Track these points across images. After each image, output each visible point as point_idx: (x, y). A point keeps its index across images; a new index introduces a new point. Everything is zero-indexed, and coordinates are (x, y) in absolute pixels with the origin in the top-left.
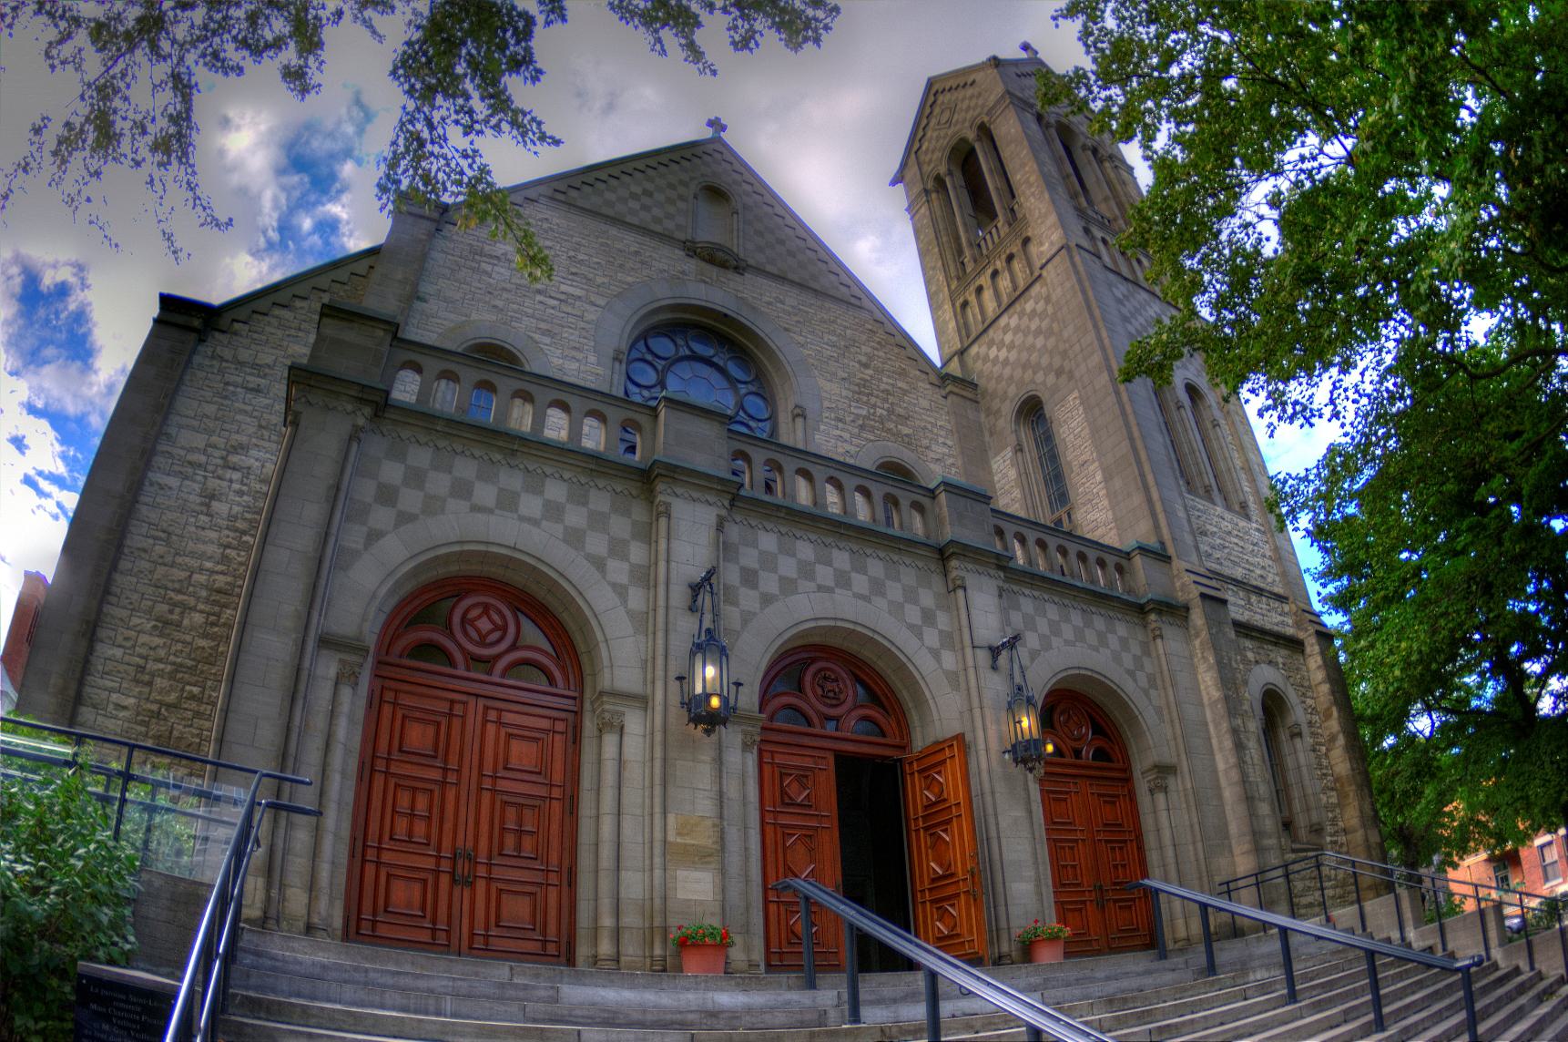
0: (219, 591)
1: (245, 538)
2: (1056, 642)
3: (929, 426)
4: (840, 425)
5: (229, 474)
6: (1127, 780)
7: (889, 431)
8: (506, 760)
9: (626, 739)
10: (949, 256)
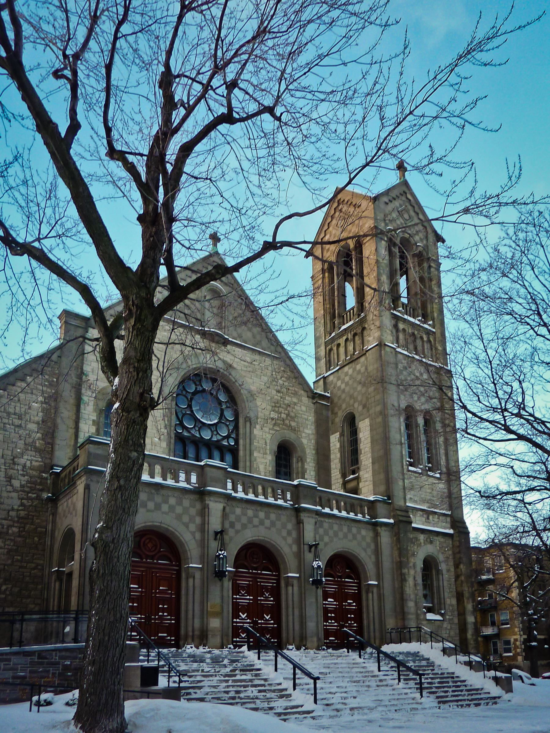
0: (22, 518)
2: (335, 539)
7: (286, 425)
9: (196, 580)
10: (328, 318)
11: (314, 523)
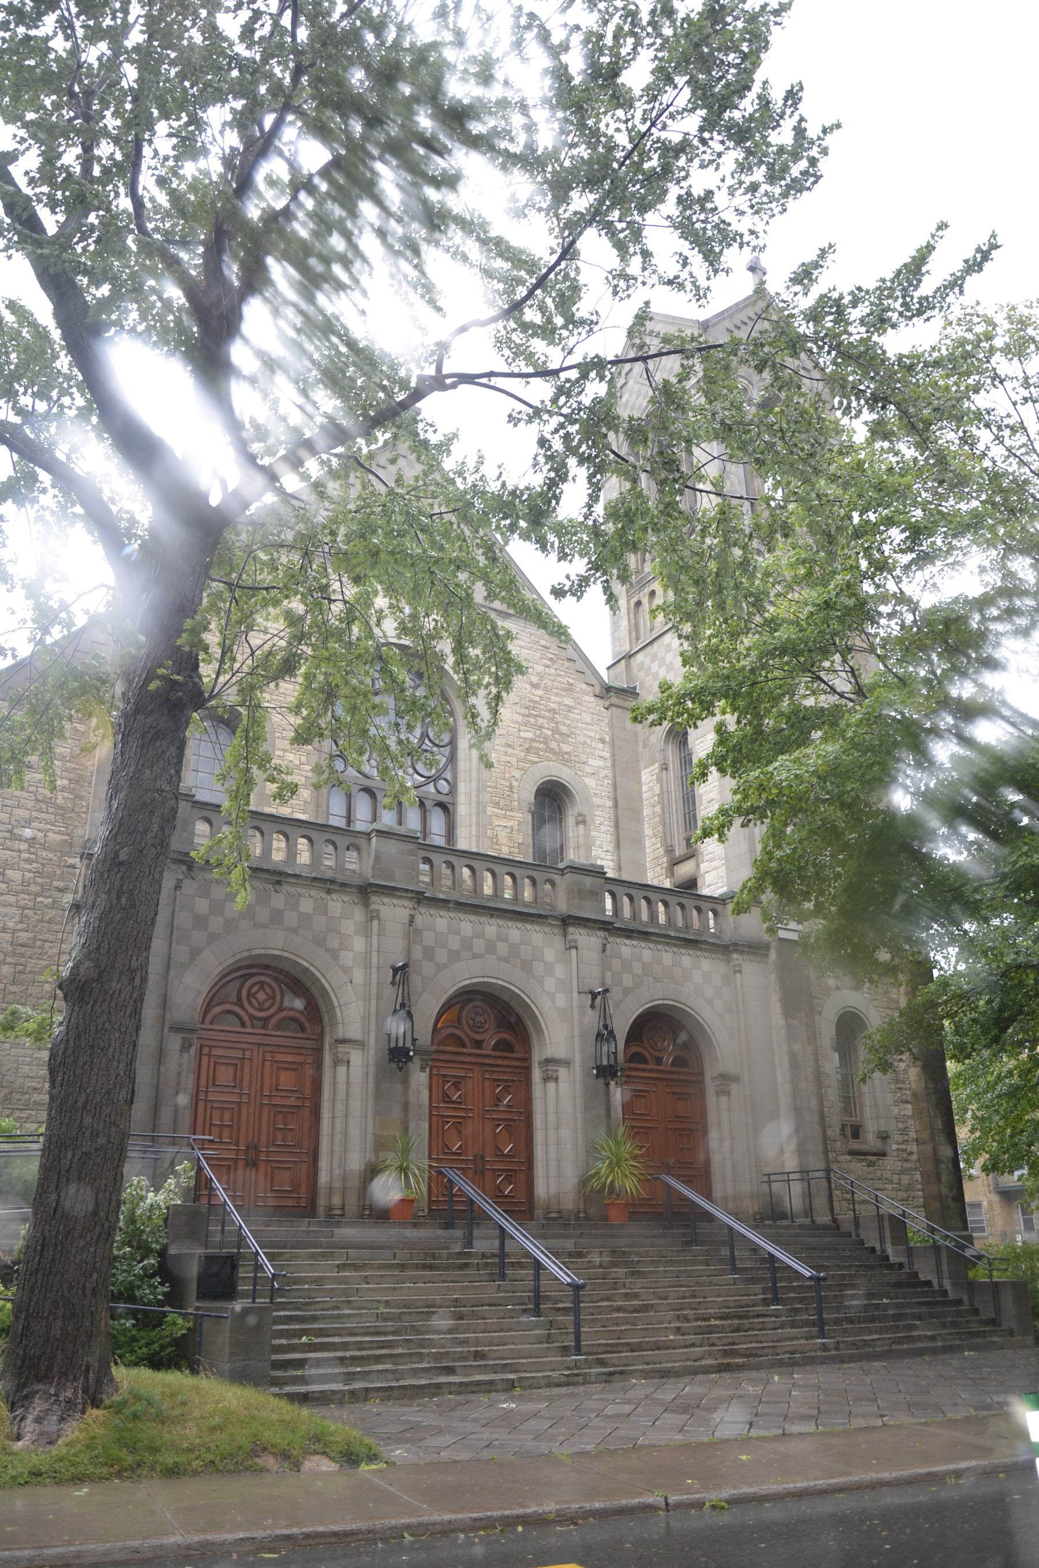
1: (39, 899)
3: (588, 741)
4: (510, 751)
5: (16, 845)
7: (552, 750)
8: (277, 1085)
9: (352, 1069)
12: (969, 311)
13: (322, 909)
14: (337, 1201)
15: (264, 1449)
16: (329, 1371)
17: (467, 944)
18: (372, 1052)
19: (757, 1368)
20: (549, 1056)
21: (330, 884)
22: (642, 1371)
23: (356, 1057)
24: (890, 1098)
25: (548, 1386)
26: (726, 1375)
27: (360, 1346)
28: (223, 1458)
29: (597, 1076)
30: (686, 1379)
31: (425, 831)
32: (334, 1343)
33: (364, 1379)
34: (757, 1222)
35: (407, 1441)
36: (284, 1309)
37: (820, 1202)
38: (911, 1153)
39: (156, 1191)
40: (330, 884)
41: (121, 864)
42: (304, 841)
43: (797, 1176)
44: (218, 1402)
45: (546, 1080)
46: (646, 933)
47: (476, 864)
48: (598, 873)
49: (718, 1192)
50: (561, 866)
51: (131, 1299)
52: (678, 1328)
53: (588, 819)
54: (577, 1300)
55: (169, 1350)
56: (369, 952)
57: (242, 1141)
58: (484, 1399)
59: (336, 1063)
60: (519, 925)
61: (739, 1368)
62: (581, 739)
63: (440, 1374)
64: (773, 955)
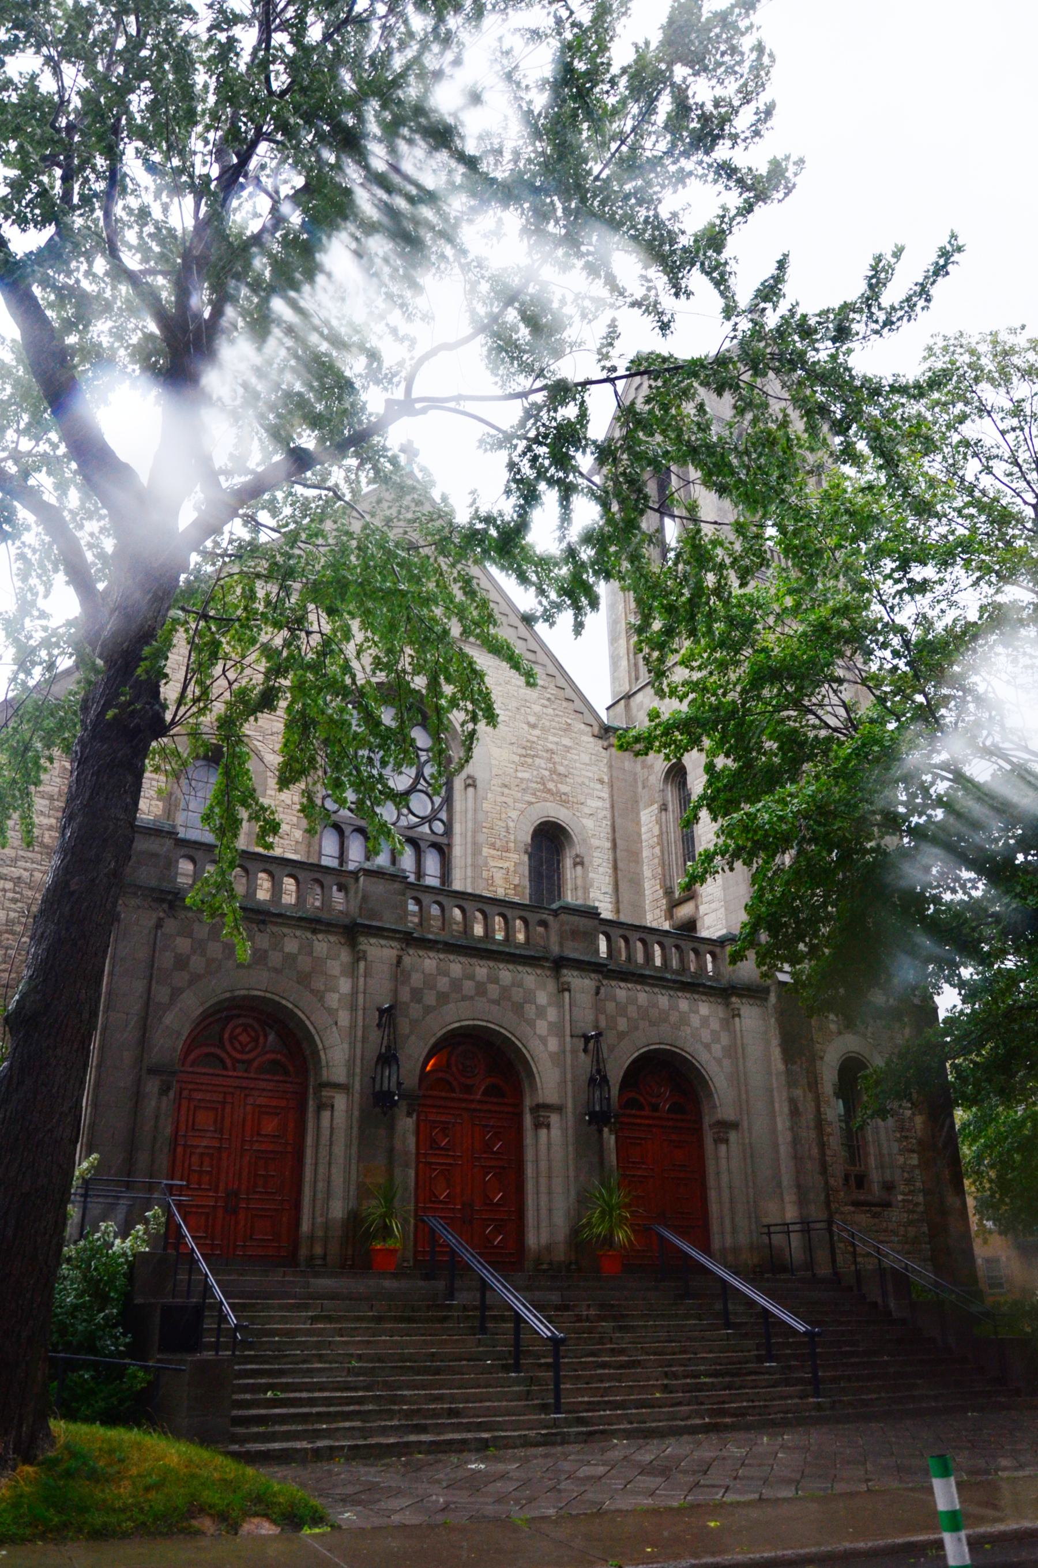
3: (587, 782)
4: (506, 791)
6: (697, 1130)
7: (549, 791)
9: (336, 1114)
11: (593, 992)
12: (952, 342)
13: (307, 949)
14: (318, 1250)
15: (202, 1510)
16: (293, 1428)
17: (456, 985)
18: (357, 1096)
19: (748, 1428)
20: (541, 1101)
21: (315, 924)
22: (624, 1430)
23: (340, 1102)
24: (895, 1147)
25: (523, 1446)
26: (714, 1437)
27: (328, 1402)
28: (156, 1518)
29: (590, 1122)
30: (672, 1440)
31: (419, 873)
32: (300, 1399)
33: (329, 1438)
34: (753, 1277)
35: (359, 1503)
36: (251, 1363)
37: (822, 1256)
38: (917, 1204)
39: (124, 1239)
40: (315, 924)
41: (72, 893)
42: (292, 881)
43: (797, 1227)
44: (158, 1460)
45: (537, 1126)
46: (642, 976)
47: (467, 905)
48: (592, 913)
49: (716, 1244)
50: (554, 906)
51: (93, 1350)
52: (666, 1386)
53: (585, 860)
54: (556, 1355)
55: (128, 1404)
56: (355, 992)
57: (222, 1187)
58: (454, 1459)
59: (320, 1107)
60: (511, 967)
61: (727, 1428)
62: (580, 780)
63: (412, 1433)
64: (773, 999)
